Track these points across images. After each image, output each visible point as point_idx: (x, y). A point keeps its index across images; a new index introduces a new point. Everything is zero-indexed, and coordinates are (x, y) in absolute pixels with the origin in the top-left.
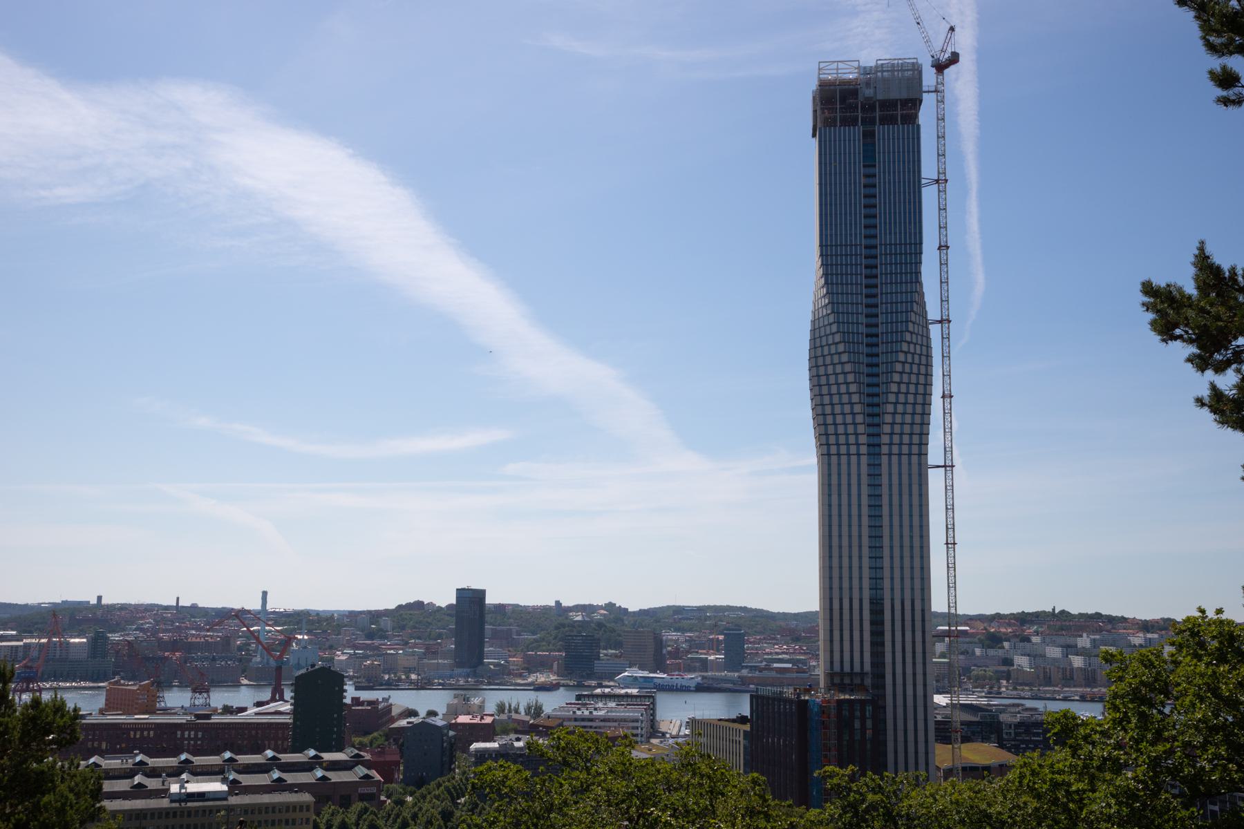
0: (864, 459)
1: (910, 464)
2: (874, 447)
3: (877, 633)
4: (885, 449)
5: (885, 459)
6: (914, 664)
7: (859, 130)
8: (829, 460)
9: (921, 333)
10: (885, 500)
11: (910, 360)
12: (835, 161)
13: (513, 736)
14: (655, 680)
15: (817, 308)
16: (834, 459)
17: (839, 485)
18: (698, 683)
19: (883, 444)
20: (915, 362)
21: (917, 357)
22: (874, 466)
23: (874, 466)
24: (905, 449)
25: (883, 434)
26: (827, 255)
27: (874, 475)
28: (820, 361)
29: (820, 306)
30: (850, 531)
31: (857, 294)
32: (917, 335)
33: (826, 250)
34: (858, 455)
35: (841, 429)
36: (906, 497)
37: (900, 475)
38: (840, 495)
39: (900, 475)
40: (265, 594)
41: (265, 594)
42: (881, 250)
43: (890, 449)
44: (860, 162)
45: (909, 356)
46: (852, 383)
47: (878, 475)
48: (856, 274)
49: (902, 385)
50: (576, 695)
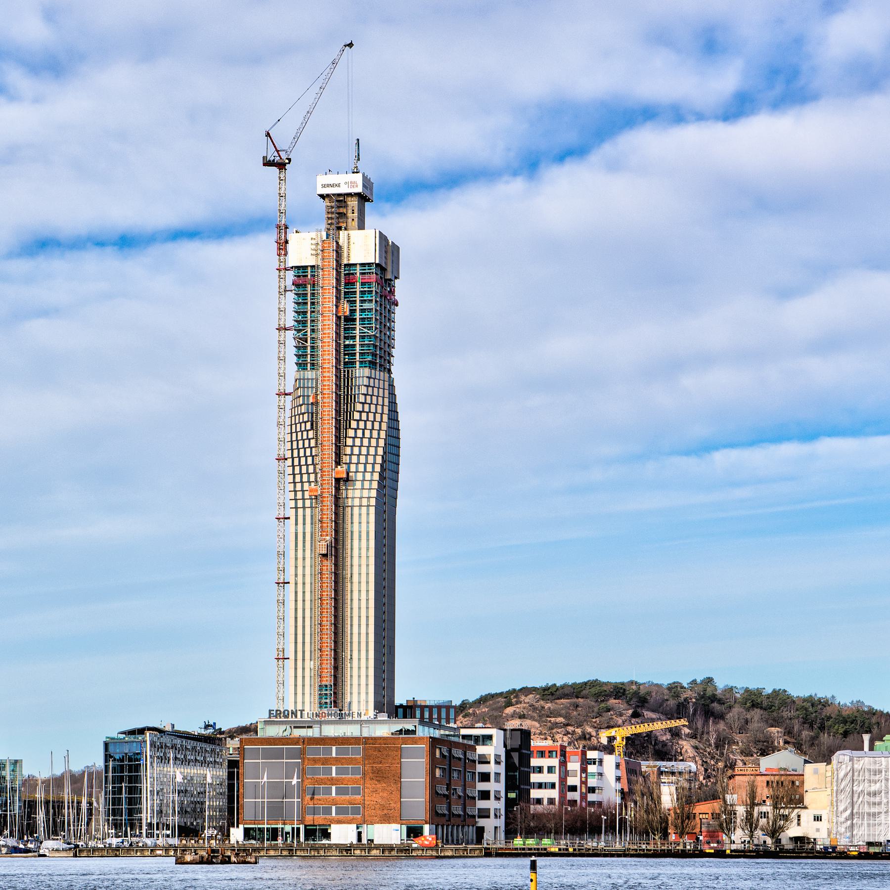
6: (359, 625)
11: (370, 393)
15: (293, 415)
20: (378, 412)
21: (374, 398)
29: (296, 406)
30: (367, 612)
32: (374, 379)
37: (304, 610)
39: (304, 610)
40: (288, 658)
41: (288, 658)
46: (307, 448)
49: (365, 405)
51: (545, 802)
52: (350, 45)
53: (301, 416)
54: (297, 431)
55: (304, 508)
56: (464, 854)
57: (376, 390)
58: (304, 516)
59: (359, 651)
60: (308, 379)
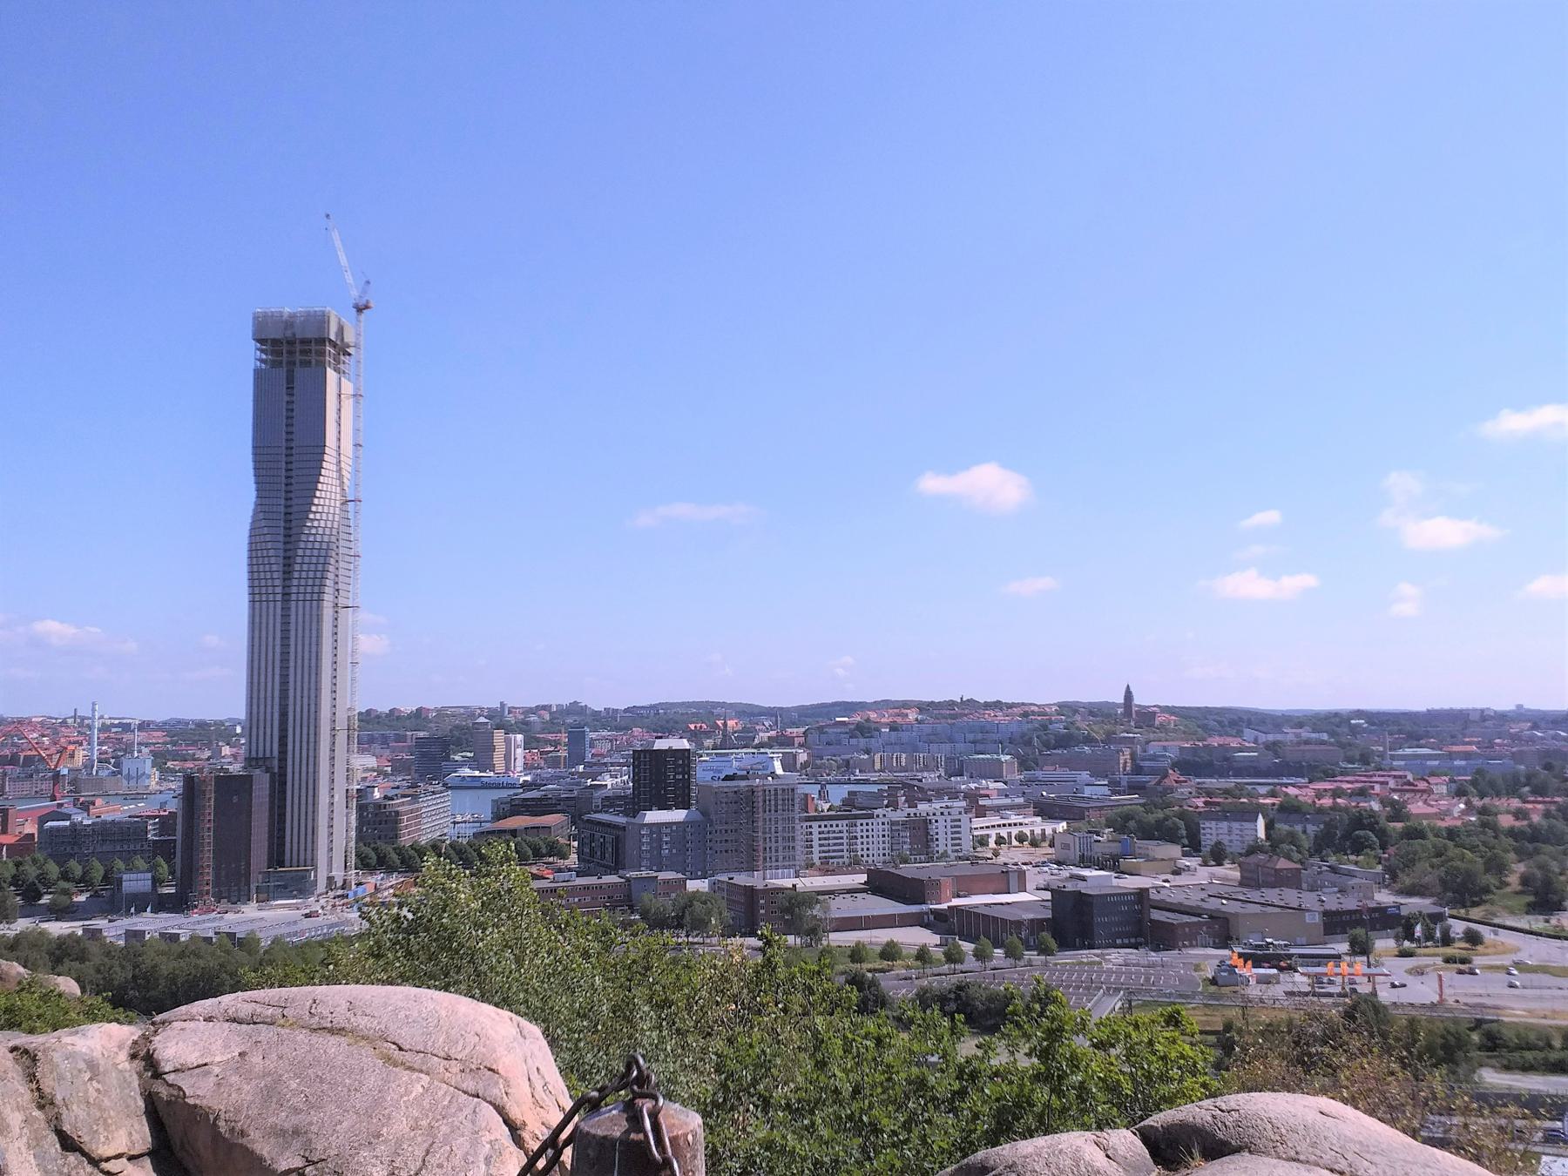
0: (279, 604)
1: (311, 607)
4: (294, 597)
6: (272, 742)
8: (254, 605)
10: (293, 633)
13: (1085, 776)
14: (483, 779)
17: (260, 623)
18: (1385, 828)
22: (286, 609)
23: (286, 609)
27: (286, 616)
36: (307, 632)
45: (324, 515)
47: (286, 660)
50: (1069, 845)
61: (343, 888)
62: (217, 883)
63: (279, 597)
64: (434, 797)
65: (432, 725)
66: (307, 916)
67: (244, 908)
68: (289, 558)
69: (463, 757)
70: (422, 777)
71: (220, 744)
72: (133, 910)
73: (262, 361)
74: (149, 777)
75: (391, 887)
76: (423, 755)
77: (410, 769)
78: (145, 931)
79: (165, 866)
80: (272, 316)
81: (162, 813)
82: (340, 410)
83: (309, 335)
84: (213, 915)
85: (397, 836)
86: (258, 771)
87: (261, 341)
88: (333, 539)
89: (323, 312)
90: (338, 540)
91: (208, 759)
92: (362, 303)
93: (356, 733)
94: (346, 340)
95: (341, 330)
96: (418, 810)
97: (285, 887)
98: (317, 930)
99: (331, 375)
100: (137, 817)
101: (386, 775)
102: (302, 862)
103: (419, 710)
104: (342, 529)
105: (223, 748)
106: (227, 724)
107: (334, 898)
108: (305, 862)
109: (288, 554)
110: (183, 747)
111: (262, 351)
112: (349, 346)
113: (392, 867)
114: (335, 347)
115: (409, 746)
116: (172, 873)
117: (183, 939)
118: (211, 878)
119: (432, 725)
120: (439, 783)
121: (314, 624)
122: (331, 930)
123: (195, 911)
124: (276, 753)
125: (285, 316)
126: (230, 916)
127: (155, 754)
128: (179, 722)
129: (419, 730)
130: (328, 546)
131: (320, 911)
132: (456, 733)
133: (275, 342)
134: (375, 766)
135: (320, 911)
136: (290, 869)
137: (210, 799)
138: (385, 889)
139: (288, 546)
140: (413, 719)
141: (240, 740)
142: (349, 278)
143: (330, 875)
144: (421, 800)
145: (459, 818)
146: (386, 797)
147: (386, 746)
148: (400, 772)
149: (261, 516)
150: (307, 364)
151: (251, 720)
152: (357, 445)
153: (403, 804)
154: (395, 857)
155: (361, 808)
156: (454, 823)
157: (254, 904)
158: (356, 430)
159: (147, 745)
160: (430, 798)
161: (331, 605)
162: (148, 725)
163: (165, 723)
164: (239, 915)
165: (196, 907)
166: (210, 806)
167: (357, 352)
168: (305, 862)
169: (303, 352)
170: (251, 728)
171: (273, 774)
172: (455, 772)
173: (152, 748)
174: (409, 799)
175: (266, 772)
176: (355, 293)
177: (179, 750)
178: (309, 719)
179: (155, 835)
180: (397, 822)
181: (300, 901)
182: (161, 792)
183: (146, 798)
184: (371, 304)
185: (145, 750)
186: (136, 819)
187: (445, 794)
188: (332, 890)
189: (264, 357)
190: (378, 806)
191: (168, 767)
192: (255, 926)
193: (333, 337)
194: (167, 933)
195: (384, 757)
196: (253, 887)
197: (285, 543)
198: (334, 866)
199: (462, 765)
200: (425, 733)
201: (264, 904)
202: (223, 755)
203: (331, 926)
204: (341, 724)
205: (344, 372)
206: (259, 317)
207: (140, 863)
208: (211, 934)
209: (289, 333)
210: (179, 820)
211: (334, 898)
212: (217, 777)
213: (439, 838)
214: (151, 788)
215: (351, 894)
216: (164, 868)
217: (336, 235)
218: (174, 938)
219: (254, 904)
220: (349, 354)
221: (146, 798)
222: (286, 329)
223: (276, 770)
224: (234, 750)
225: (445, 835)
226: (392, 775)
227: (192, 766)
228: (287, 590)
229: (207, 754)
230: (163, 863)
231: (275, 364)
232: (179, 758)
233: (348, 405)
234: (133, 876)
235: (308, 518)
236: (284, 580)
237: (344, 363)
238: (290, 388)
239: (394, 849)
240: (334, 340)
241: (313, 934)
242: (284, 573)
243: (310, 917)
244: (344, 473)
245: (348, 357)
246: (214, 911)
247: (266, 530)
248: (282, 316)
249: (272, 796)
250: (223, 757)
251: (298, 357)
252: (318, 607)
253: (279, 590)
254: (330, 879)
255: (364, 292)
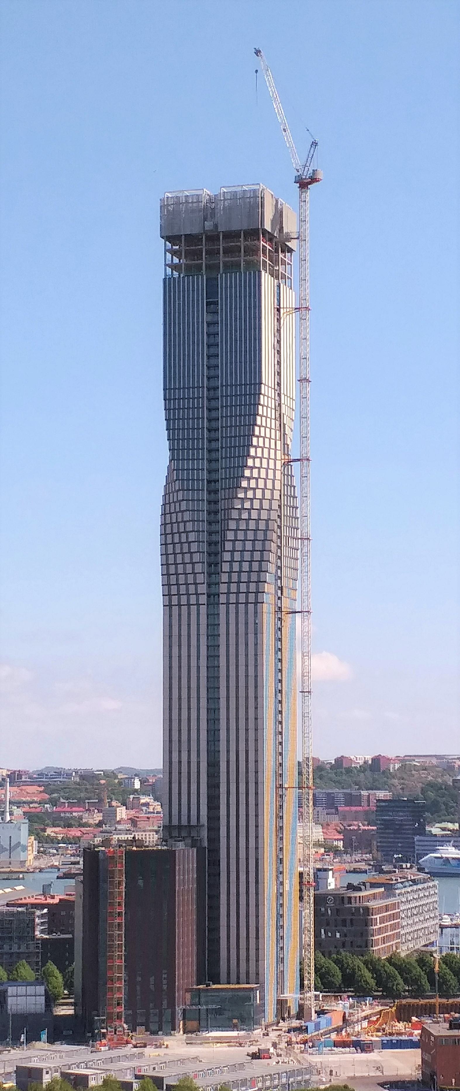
0: (203, 609)
2: (213, 597)
3: (213, 786)
4: (223, 599)
5: (223, 608)
7: (202, 277)
9: (268, 425)
12: (179, 299)
15: (168, 492)
16: (175, 610)
19: (222, 593)
21: (265, 461)
22: (213, 616)
23: (213, 616)
24: (242, 598)
25: (221, 583)
26: (170, 400)
27: (213, 626)
28: (172, 569)
31: (198, 490)
33: (174, 434)
34: (198, 605)
35: (182, 579)
38: (180, 646)
42: (222, 423)
43: (229, 588)
44: (202, 299)
47: (214, 688)
48: (198, 449)
51: (375, 1036)
52: (257, 71)
53: (177, 504)
54: (178, 535)
55: (179, 605)
56: (120, 914)
57: (259, 450)
58: (180, 615)
59: (228, 762)
60: (193, 490)
61: (299, 1016)
62: (130, 1004)
63: (203, 599)
64: (415, 888)
65: (396, 781)
66: (255, 1056)
67: (168, 1040)
68: (216, 543)
69: (443, 829)
70: (388, 859)
71: (114, 803)
72: (23, 1038)
73: (174, 267)
74: (25, 849)
75: (365, 1018)
76: (386, 825)
77: (370, 845)
78: (42, 1069)
79: (59, 975)
80: (187, 202)
81: (50, 901)
82: (279, 331)
83: (235, 226)
84: (128, 1050)
85: (367, 944)
86: (181, 846)
87: (168, 238)
88: (274, 515)
89: (254, 191)
90: (279, 517)
91: (100, 824)
92: (307, 174)
93: (311, 792)
94: (285, 230)
95: (279, 216)
96: (394, 906)
97: (218, 1012)
98: (272, 1079)
99: (267, 281)
100: (21, 905)
101: (337, 852)
102: (243, 976)
103: (376, 760)
104: (284, 501)
105: (118, 809)
106: (120, 776)
107: (289, 1031)
108: (238, 978)
109: (214, 538)
110: (67, 809)
111: (174, 253)
112: (289, 239)
113: (364, 990)
114: (271, 240)
115: (366, 813)
116: (69, 985)
117: (92, 1083)
118: (122, 996)
119: (396, 781)
120: (411, 867)
121: (251, 637)
122: (291, 1080)
123: (104, 1041)
124: (204, 820)
125: (204, 200)
126: (149, 1051)
127: (31, 817)
128: (59, 773)
129: (379, 789)
130: (267, 525)
131: (272, 1050)
132: (431, 794)
133: (191, 239)
134: (321, 838)
135: (272, 1050)
136: (228, 986)
137: (120, 883)
138: (358, 1021)
139: (214, 527)
140: (368, 773)
141: (139, 799)
142: (289, 138)
143: (282, 997)
144: (398, 891)
145: (447, 921)
146: (350, 887)
147: (333, 810)
148: (356, 849)
149: (177, 485)
150: (232, 267)
151: (170, 773)
152: (303, 380)
153: (374, 897)
154: (368, 975)
155: (320, 900)
156: (442, 927)
157: (180, 1035)
158: (303, 359)
159: (19, 804)
160: (409, 889)
161: (272, 609)
162: (20, 776)
163: (41, 774)
164: (161, 1051)
165: (104, 1035)
166: (120, 893)
167: (300, 247)
168: (238, 978)
169: (227, 251)
170: (170, 783)
171: (200, 851)
172: (435, 851)
173: (26, 808)
174: (382, 889)
175: (192, 847)
176: (297, 161)
177: (60, 812)
178: (247, 772)
179: (42, 932)
180: (367, 923)
181: (242, 1033)
182: (41, 870)
183: (23, 879)
184: (320, 175)
185: (18, 812)
186: (20, 909)
187: (431, 884)
188: (284, 1019)
189: (176, 260)
190: (340, 899)
191: (49, 836)
192: (190, 1068)
193: (268, 227)
194: (72, 1074)
195: (332, 826)
196: (179, 1010)
197: (210, 523)
198: (287, 984)
199: (444, 840)
200: (387, 793)
201: (193, 1035)
202: (118, 819)
203: (290, 1074)
204: (290, 780)
205: (284, 277)
206: (168, 205)
207: (26, 971)
208: (129, 1078)
209: (209, 225)
210: (78, 912)
211: (289, 1031)
212: (129, 854)
213: (424, 949)
214: (27, 864)
215: (311, 1026)
216: (58, 979)
217: (269, 79)
218: (81, 1081)
219: (180, 1035)
220: (290, 250)
221: (23, 879)
222: (205, 219)
223: (206, 844)
224: (132, 812)
225: (432, 944)
226: (346, 853)
227: (79, 834)
228: (213, 590)
229: (98, 817)
230: (57, 972)
231: (192, 270)
232: (62, 823)
233: (289, 321)
234: (22, 990)
235: (240, 487)
236: (210, 575)
237: (284, 263)
238: (212, 304)
239: (366, 963)
240: (270, 231)
241: (268, 1083)
242: (210, 565)
243: (259, 1058)
244: (286, 420)
245: (288, 255)
246: (128, 1043)
247: (184, 506)
248: (198, 202)
249: (200, 880)
250: (119, 822)
251: (222, 258)
252: (256, 612)
253: (203, 589)
254: (281, 1004)
255: (310, 157)
